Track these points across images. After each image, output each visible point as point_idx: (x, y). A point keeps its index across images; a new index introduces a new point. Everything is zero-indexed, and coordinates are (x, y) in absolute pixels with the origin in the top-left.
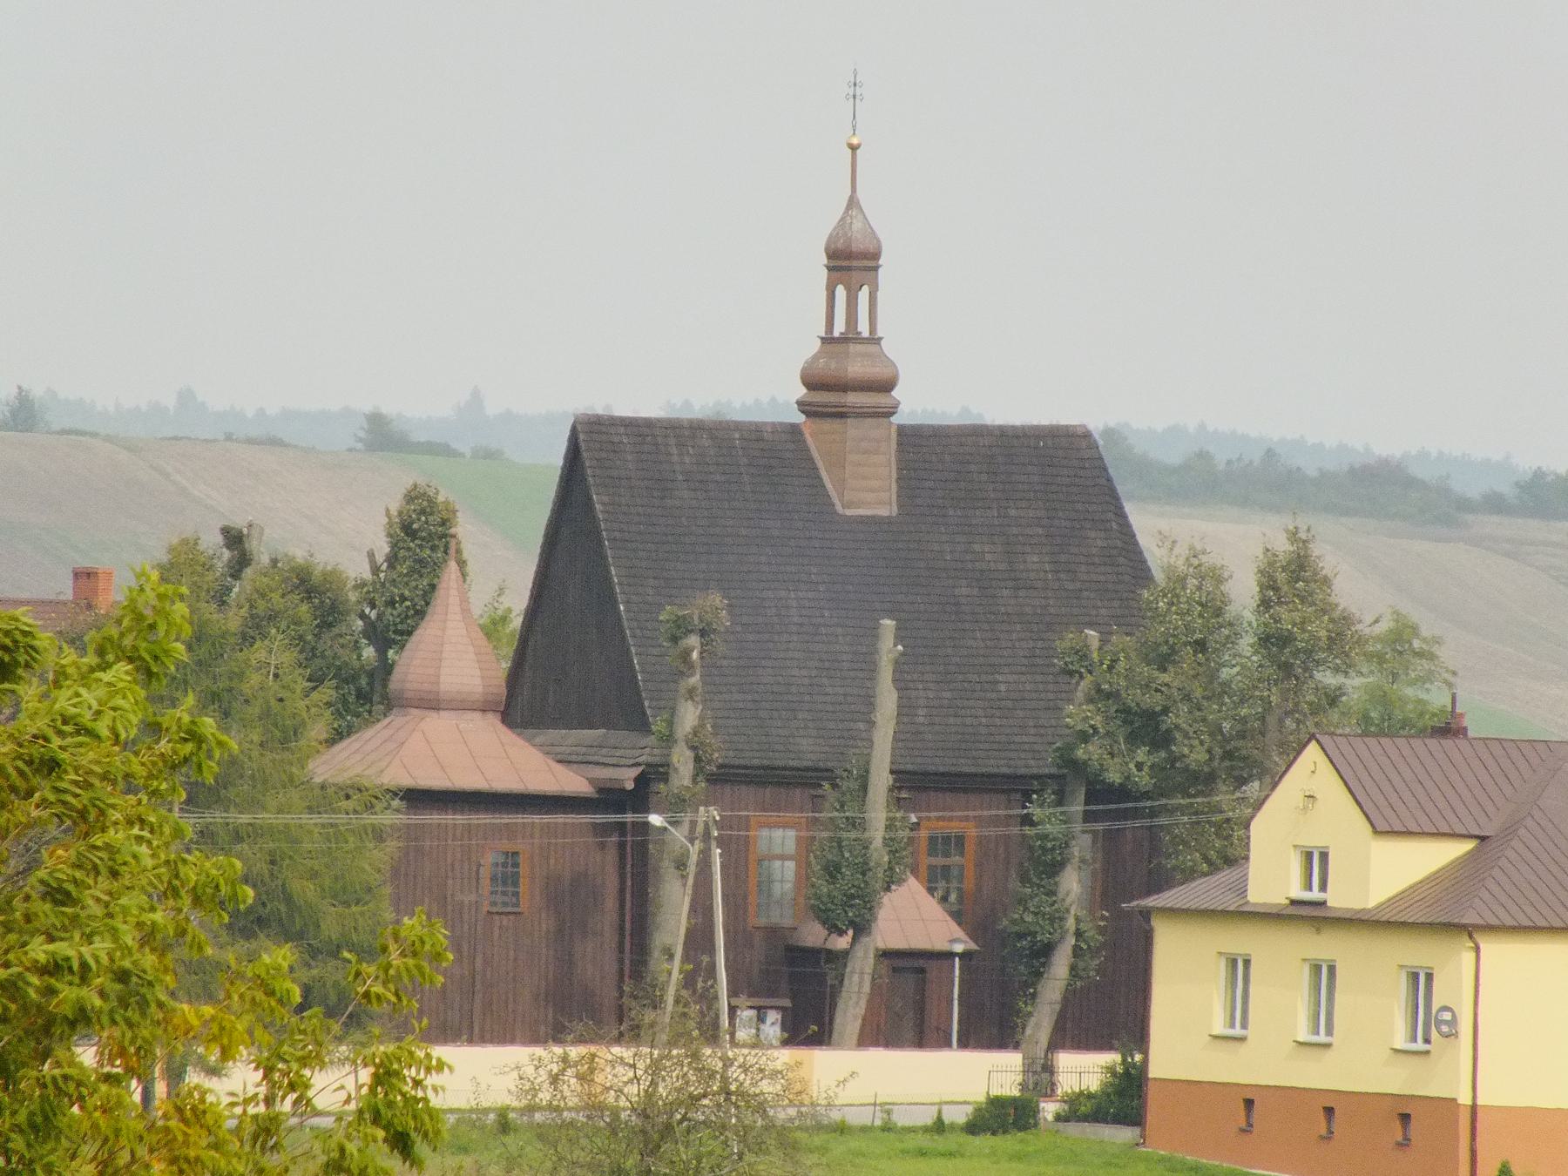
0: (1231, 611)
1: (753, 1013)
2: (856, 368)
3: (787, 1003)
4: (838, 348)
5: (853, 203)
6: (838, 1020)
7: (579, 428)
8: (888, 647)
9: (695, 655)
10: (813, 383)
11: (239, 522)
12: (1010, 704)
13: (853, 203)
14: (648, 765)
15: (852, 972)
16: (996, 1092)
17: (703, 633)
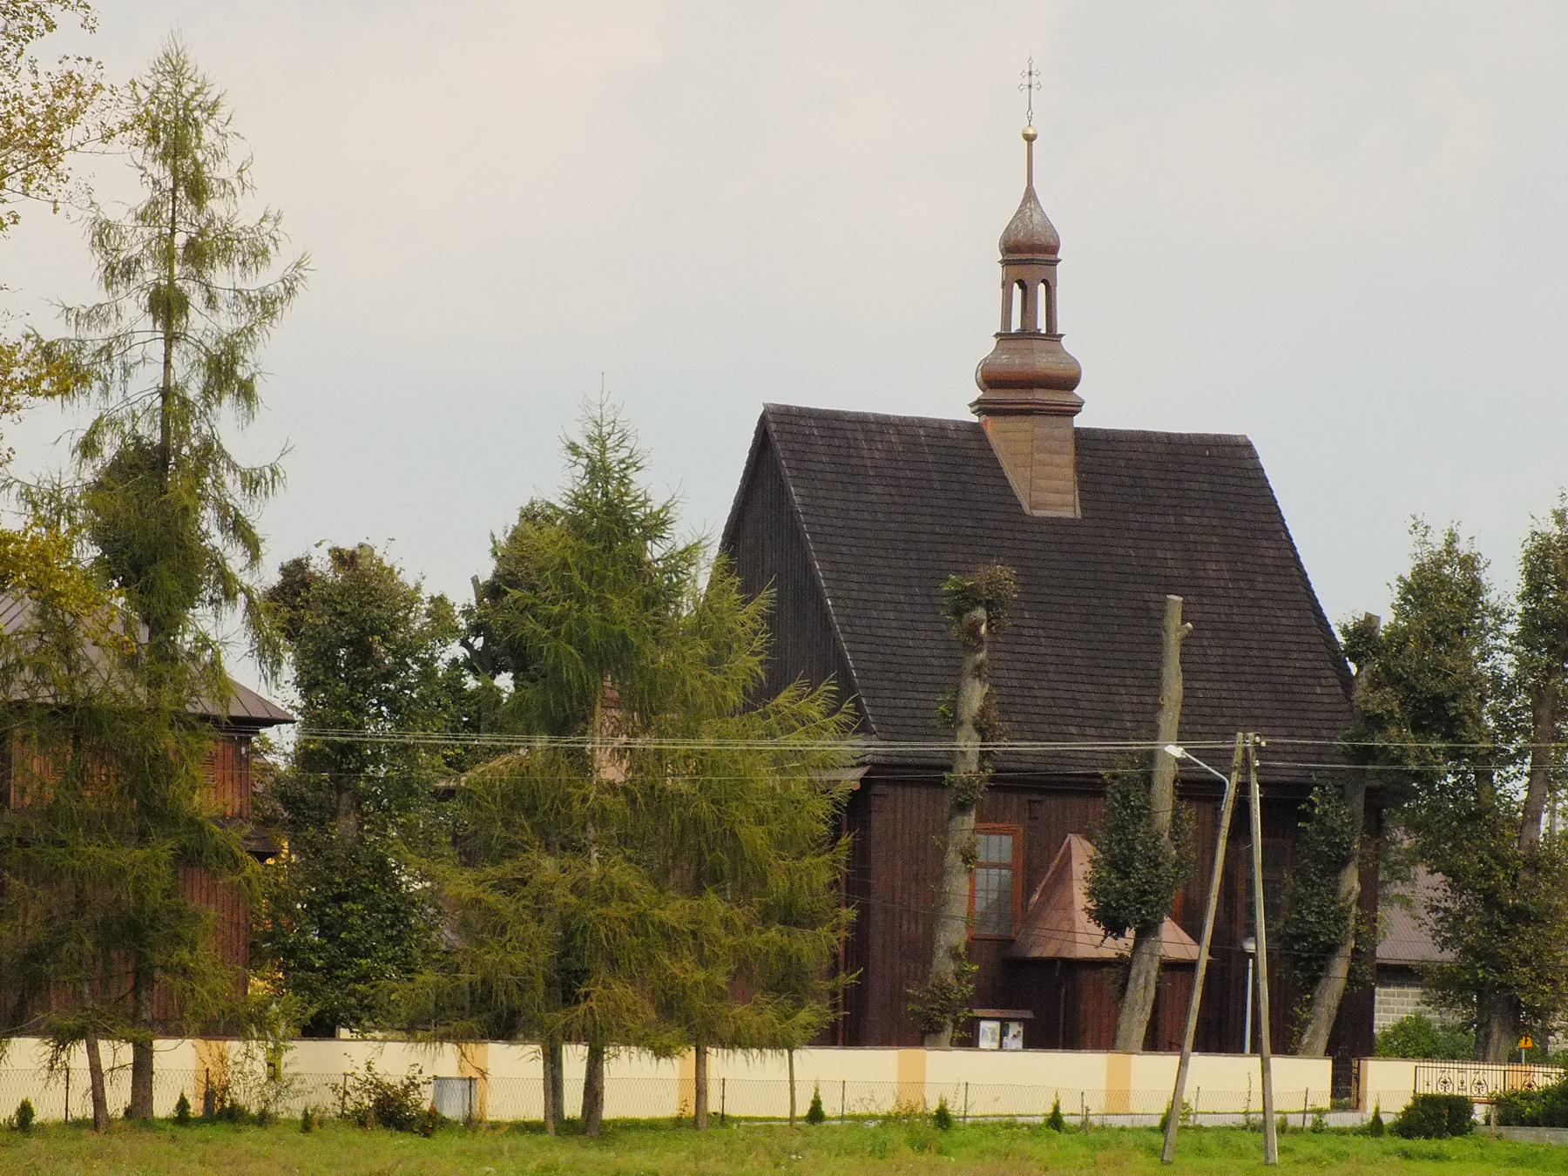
0: (1490, 598)
1: (996, 1025)
2: (1042, 363)
3: (1028, 1015)
4: (1012, 344)
5: (1030, 195)
6: (1123, 1027)
7: (770, 417)
8: (1176, 628)
9: (983, 629)
10: (991, 380)
11: (349, 545)
12: (1208, 711)
13: (1030, 195)
14: (874, 765)
15: (1138, 975)
16: (1423, 1090)
17: (989, 605)
